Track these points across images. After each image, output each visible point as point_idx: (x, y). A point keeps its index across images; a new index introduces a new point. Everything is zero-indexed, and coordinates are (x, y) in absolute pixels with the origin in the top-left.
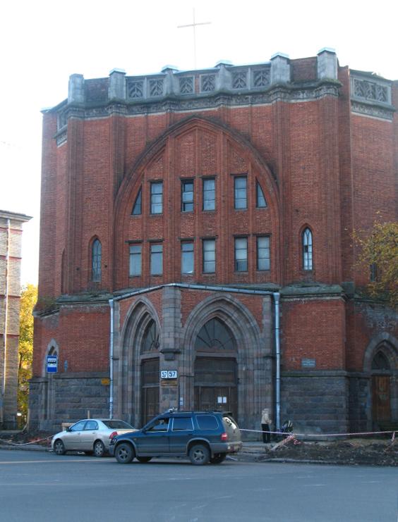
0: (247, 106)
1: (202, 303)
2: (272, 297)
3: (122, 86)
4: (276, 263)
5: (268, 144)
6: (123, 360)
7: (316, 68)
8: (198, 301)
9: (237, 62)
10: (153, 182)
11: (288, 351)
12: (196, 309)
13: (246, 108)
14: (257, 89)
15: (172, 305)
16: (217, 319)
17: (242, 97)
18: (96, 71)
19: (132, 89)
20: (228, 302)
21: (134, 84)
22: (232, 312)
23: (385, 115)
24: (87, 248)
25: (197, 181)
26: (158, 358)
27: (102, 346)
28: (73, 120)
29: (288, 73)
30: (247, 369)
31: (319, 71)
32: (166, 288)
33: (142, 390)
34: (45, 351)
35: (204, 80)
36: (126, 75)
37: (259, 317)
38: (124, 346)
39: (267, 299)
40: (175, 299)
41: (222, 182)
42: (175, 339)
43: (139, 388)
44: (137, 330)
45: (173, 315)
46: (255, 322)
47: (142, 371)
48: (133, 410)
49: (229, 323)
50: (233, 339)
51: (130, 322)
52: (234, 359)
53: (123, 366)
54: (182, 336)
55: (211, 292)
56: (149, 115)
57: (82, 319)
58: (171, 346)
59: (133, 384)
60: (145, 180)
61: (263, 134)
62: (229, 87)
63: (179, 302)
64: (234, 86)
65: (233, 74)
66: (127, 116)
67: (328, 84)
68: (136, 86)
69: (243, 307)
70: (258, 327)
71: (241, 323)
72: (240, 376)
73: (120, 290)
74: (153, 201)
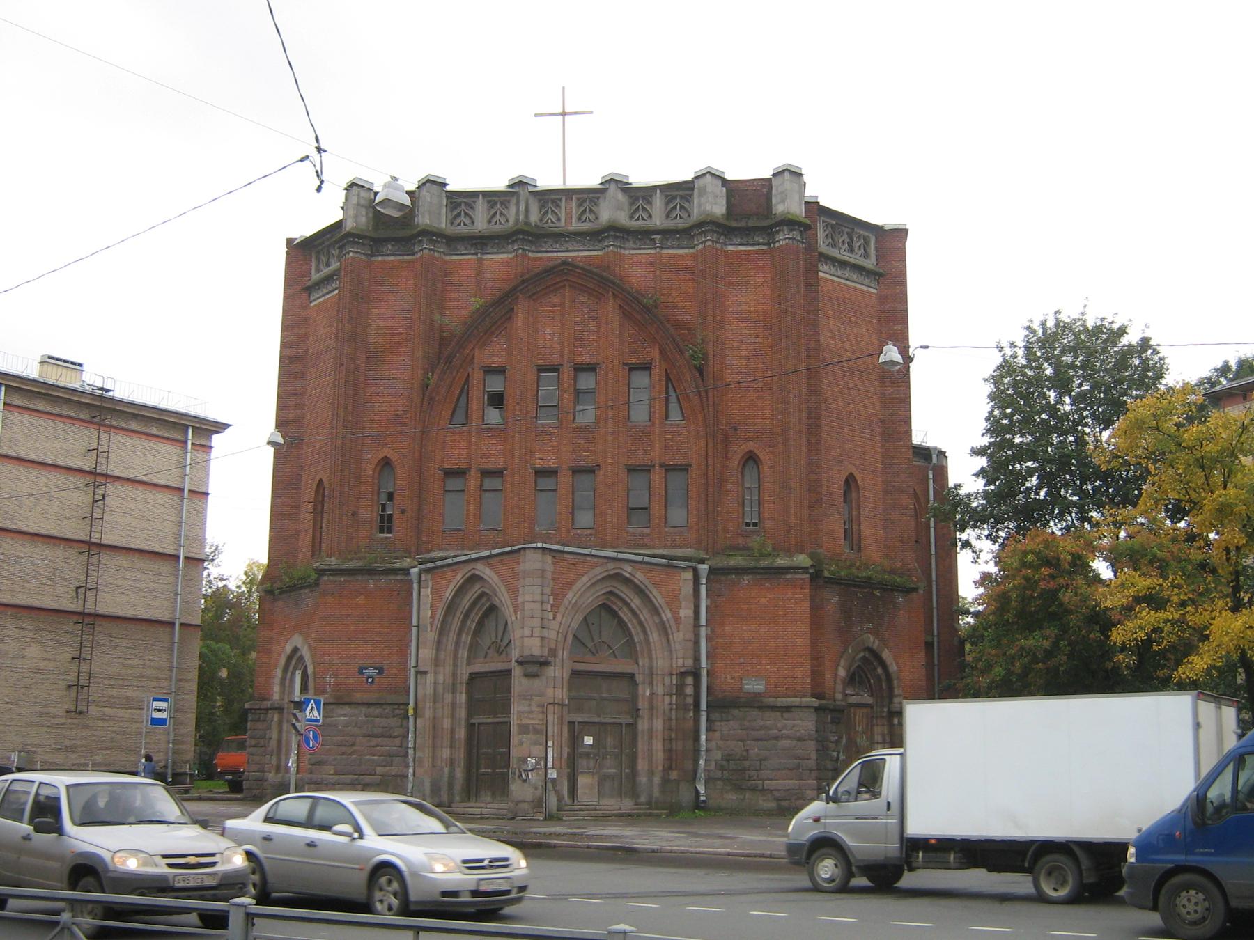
0: (653, 251)
1: (585, 579)
2: (695, 570)
3: (440, 206)
6: (435, 673)
7: (768, 197)
8: (579, 576)
9: (639, 178)
10: (489, 371)
11: (720, 664)
12: (575, 588)
14: (670, 224)
15: (538, 581)
17: (644, 235)
19: (456, 212)
21: (460, 205)
23: (867, 281)
25: (567, 371)
26: (507, 673)
28: (353, 258)
29: (724, 202)
30: (652, 694)
31: (774, 201)
32: (529, 554)
33: (471, 727)
35: (580, 205)
36: (448, 188)
38: (437, 650)
39: (689, 576)
40: (543, 571)
41: (610, 376)
42: (542, 638)
44: (464, 622)
45: (538, 598)
46: (669, 615)
48: (452, 762)
49: (625, 615)
50: (630, 643)
51: (451, 608)
52: (631, 677)
54: (553, 635)
56: (485, 257)
57: (360, 600)
58: (536, 652)
59: (453, 716)
60: (476, 367)
61: (679, 300)
62: (623, 219)
63: (549, 575)
64: (631, 217)
65: (631, 197)
66: (448, 258)
67: (790, 223)
68: (463, 206)
69: (650, 586)
70: (672, 622)
71: (645, 615)
73: (428, 552)
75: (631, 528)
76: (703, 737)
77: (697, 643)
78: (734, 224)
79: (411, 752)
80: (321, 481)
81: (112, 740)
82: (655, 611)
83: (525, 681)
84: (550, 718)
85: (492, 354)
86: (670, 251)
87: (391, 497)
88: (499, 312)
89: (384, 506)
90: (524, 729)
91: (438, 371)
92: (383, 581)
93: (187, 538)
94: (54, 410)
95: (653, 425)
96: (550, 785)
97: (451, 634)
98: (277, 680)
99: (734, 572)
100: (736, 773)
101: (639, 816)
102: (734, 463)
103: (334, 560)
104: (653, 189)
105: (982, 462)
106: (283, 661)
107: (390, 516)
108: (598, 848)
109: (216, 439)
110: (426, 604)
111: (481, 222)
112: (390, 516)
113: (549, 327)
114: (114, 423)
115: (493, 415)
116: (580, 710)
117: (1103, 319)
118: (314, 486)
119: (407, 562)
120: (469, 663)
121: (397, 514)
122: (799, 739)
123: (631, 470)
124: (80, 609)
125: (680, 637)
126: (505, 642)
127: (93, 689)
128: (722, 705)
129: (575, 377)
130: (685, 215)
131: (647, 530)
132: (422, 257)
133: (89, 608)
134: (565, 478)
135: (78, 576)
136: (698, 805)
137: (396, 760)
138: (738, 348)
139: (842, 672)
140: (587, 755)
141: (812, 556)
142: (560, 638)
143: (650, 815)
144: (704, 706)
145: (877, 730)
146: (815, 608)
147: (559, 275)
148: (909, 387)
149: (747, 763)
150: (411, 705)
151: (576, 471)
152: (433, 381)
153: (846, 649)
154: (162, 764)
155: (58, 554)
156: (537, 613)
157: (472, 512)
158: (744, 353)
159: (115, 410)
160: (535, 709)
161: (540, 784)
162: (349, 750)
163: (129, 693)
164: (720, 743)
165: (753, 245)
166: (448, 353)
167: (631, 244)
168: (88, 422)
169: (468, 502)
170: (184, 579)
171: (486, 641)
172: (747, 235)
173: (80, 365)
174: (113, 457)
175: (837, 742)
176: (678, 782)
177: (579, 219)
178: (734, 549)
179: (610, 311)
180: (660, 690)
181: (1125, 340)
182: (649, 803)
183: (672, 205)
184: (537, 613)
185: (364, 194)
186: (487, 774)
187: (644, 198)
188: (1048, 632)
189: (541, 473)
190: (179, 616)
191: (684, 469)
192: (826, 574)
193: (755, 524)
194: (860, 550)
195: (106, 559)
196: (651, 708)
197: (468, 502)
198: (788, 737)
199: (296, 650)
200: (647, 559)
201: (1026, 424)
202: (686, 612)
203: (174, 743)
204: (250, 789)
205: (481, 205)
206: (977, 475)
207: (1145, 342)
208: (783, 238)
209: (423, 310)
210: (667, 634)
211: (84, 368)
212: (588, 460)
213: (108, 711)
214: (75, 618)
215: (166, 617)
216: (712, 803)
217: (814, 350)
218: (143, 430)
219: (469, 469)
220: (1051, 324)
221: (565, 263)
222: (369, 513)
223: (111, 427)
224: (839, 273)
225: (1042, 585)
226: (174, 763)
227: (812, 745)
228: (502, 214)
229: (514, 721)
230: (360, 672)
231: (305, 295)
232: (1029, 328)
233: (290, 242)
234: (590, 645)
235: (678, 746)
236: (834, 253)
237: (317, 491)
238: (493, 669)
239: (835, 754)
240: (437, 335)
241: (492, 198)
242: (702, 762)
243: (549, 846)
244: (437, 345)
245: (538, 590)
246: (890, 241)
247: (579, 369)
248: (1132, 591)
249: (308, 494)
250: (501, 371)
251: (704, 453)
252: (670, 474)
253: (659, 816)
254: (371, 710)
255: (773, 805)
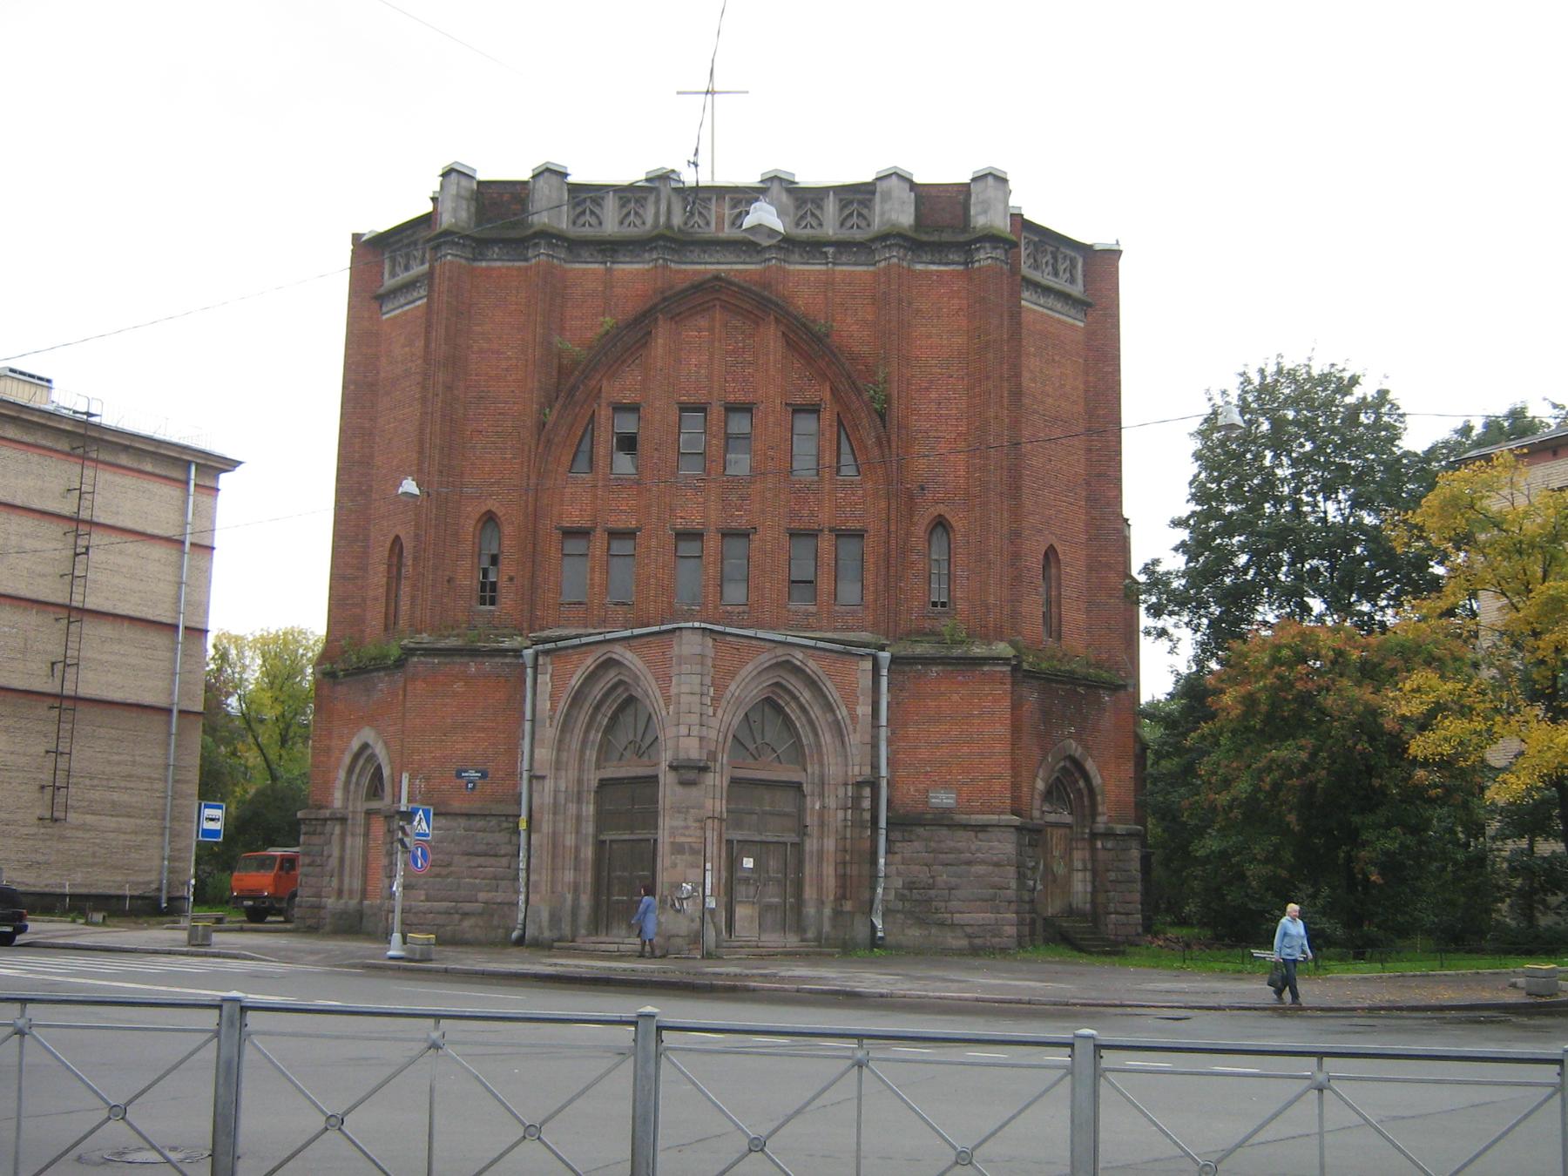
0: (823, 268)
1: (750, 667)
2: (875, 659)
4: (876, 591)
5: (866, 348)
7: (966, 206)
8: (743, 663)
9: (809, 175)
10: (619, 408)
11: (902, 773)
12: (738, 678)
13: (826, 272)
14: (845, 235)
15: (698, 668)
16: (770, 704)
17: (813, 247)
18: (504, 162)
19: (579, 210)
20: (795, 666)
21: (584, 200)
22: (800, 686)
23: (1073, 312)
24: (470, 538)
25: (716, 411)
26: (653, 780)
27: (502, 748)
28: (451, 262)
29: (912, 209)
30: (823, 807)
31: (972, 212)
32: (686, 635)
33: (600, 845)
34: (343, 752)
36: (570, 179)
37: (851, 700)
38: (559, 750)
39: (868, 665)
40: (703, 656)
41: (771, 419)
42: (701, 739)
43: (590, 840)
45: (697, 689)
46: (844, 709)
47: (598, 804)
49: (792, 711)
50: (798, 745)
51: (577, 698)
52: (798, 787)
53: (556, 791)
54: (713, 734)
55: (768, 645)
57: (458, 687)
61: (853, 330)
63: (709, 662)
64: (798, 224)
66: (568, 266)
67: (993, 239)
68: (588, 203)
70: (848, 721)
71: (816, 712)
72: (808, 821)
73: (542, 629)
74: (814, 459)
75: (793, 606)
76: (882, 861)
77: (875, 746)
78: (925, 238)
79: (523, 875)
80: (397, 537)
81: (94, 855)
82: (829, 707)
83: (679, 790)
84: (709, 834)
85: (624, 386)
86: (845, 268)
87: (494, 560)
88: (633, 335)
89: (485, 573)
90: (678, 849)
91: (557, 406)
92: (488, 664)
93: (188, 603)
94: (26, 438)
95: (821, 480)
96: (707, 916)
97: (576, 731)
98: (339, 784)
99: (924, 661)
100: (919, 904)
101: (807, 955)
102: (920, 530)
103: (425, 637)
104: (825, 190)
105: (1184, 535)
106: (347, 759)
107: (494, 584)
108: (810, 991)
109: (224, 478)
110: (545, 693)
111: (611, 223)
112: (494, 584)
113: (694, 357)
114: (102, 457)
115: (624, 464)
116: (738, 825)
117: (1333, 365)
118: (388, 545)
119: (517, 642)
120: (598, 767)
121: (503, 583)
122: (997, 865)
123: (793, 534)
124: (57, 690)
125: (857, 739)
126: (648, 741)
127: (72, 790)
128: (904, 823)
129: (726, 417)
130: (863, 224)
131: (813, 609)
132: (538, 265)
133: (69, 690)
134: (712, 542)
135: (57, 651)
136: (874, 942)
137: (503, 883)
138: (927, 389)
139: (1040, 785)
140: (747, 880)
141: (1013, 644)
142: (721, 739)
143: (820, 954)
144: (883, 823)
145: (1077, 855)
146: (1016, 707)
147: (710, 292)
148: (1120, 443)
149: (932, 892)
150: (524, 817)
151: (727, 534)
152: (551, 418)
153: (1045, 758)
154: (154, 886)
155: (33, 618)
156: (690, 706)
157: (597, 580)
158: (933, 395)
159: (103, 440)
160: (691, 823)
161: (698, 914)
162: (444, 871)
163: (115, 796)
164: (902, 867)
165: (947, 264)
166: (569, 385)
167: (796, 257)
168: (68, 454)
169: (593, 569)
170: (185, 654)
171: (622, 738)
172: (940, 252)
173: (49, 381)
174: (98, 499)
175: (1034, 869)
176: (852, 914)
177: (733, 224)
178: (921, 634)
179: (771, 338)
180: (831, 803)
181: (1358, 392)
182: (818, 939)
183: (847, 212)
184: (690, 706)
185: (464, 182)
186: (622, 902)
187: (813, 201)
188: (1303, 742)
189: (683, 535)
190: (178, 702)
191: (859, 535)
192: (1025, 666)
193: (943, 604)
194: (1059, 638)
195: (90, 629)
196: (822, 825)
197: (593, 569)
198: (983, 862)
199: (365, 746)
200: (821, 644)
201: (1235, 494)
202: (864, 710)
203: (171, 859)
204: (302, 918)
205: (611, 203)
206: (1176, 549)
207: (1383, 395)
208: (985, 257)
209: (527, 332)
210: (841, 735)
211: (54, 384)
212: (740, 521)
213: (89, 819)
214: (50, 701)
215: (160, 700)
216: (890, 940)
217: (1017, 394)
218: (135, 465)
219: (593, 529)
220: (1271, 369)
221: (717, 278)
222: (468, 580)
223: (97, 461)
224: (1042, 301)
225: (1299, 686)
226: (169, 884)
227: (1011, 871)
228: (636, 213)
229: (664, 838)
230: (459, 776)
231: (375, 305)
232: (1243, 374)
233: (356, 238)
234: (752, 747)
235: (853, 870)
236: (1036, 276)
237: (391, 550)
238: (784, 778)
239: (1031, 883)
240: (556, 361)
241: (629, 195)
242: (880, 890)
243: (747, 989)
244: (555, 373)
245: (697, 679)
246: (1100, 265)
247: (731, 408)
248: (1432, 697)
249: (380, 553)
250: (634, 408)
251: (884, 516)
252: (841, 540)
253: (832, 955)
254: (472, 822)
255: (964, 943)
